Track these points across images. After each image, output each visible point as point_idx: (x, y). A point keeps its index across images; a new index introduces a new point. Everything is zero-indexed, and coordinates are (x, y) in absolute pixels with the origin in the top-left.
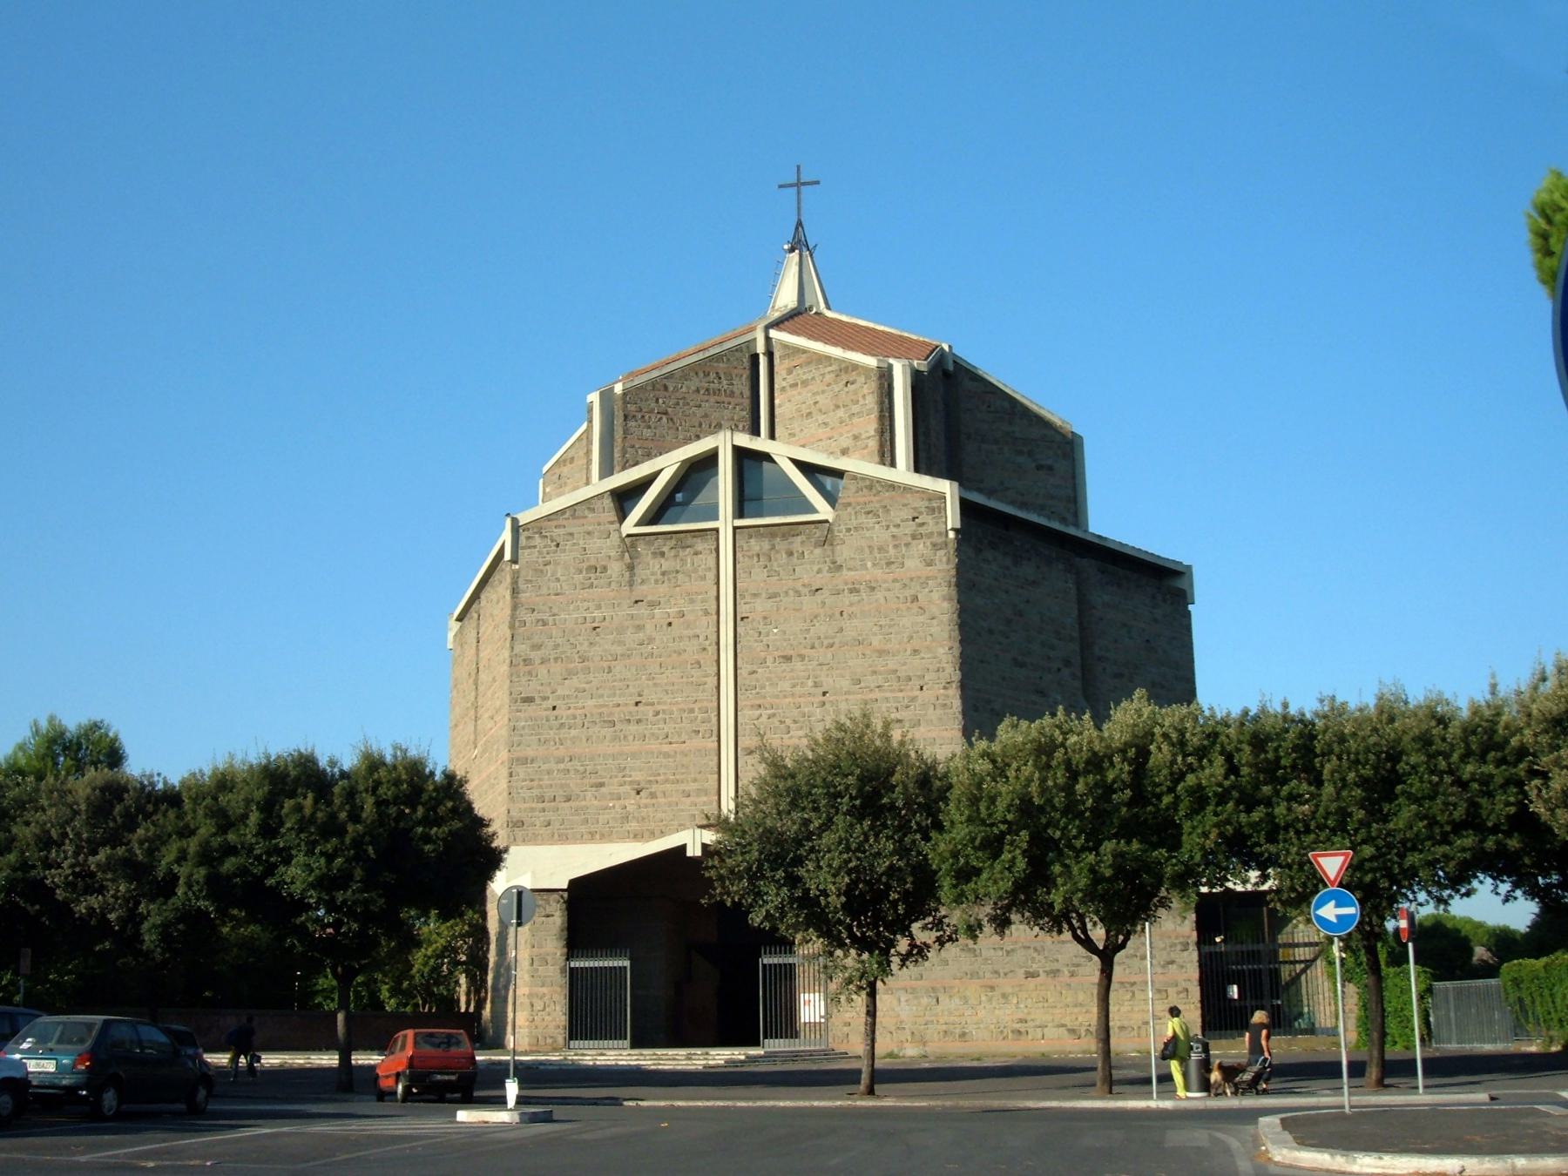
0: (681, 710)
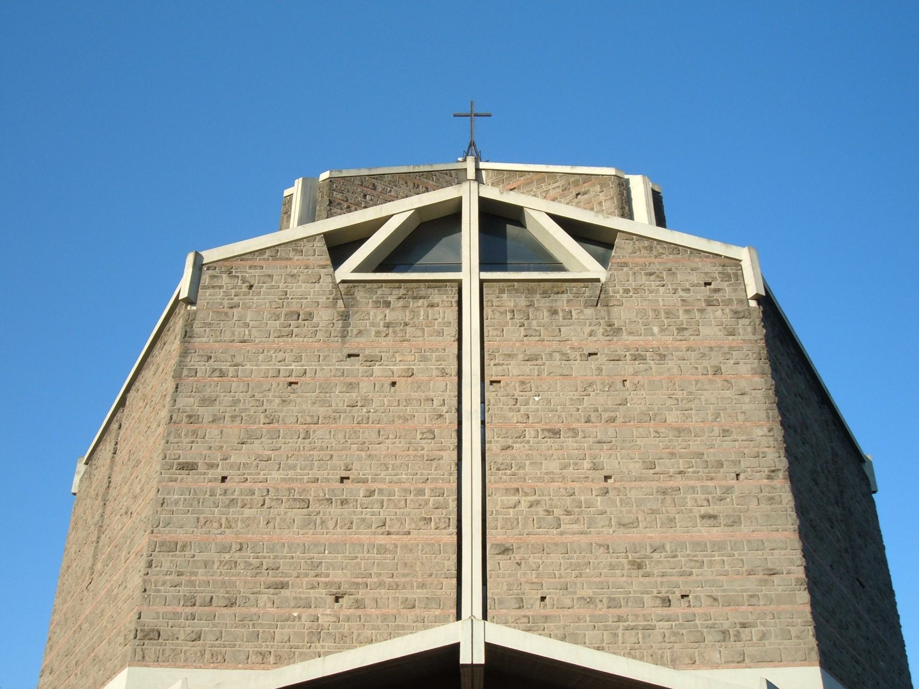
0: (405, 490)
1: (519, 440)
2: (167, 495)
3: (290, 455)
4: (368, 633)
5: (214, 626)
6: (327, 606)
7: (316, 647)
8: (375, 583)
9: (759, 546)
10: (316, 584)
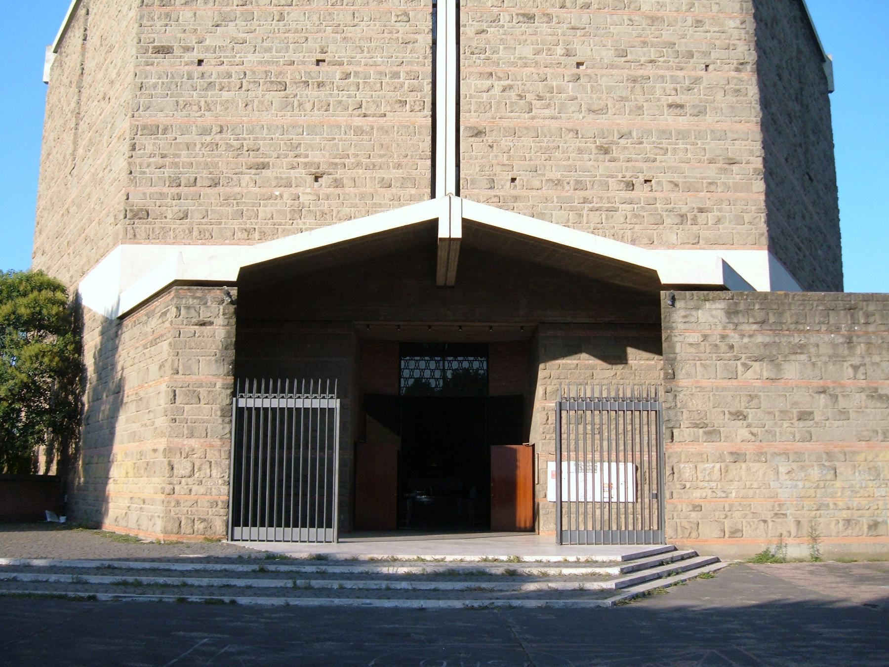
0: (381, 73)
1: (494, 24)
2: (145, 79)
3: (265, 38)
4: (346, 210)
5: (200, 205)
6: (308, 186)
7: (297, 224)
8: (353, 164)
9: (722, 136)
10: (296, 165)
